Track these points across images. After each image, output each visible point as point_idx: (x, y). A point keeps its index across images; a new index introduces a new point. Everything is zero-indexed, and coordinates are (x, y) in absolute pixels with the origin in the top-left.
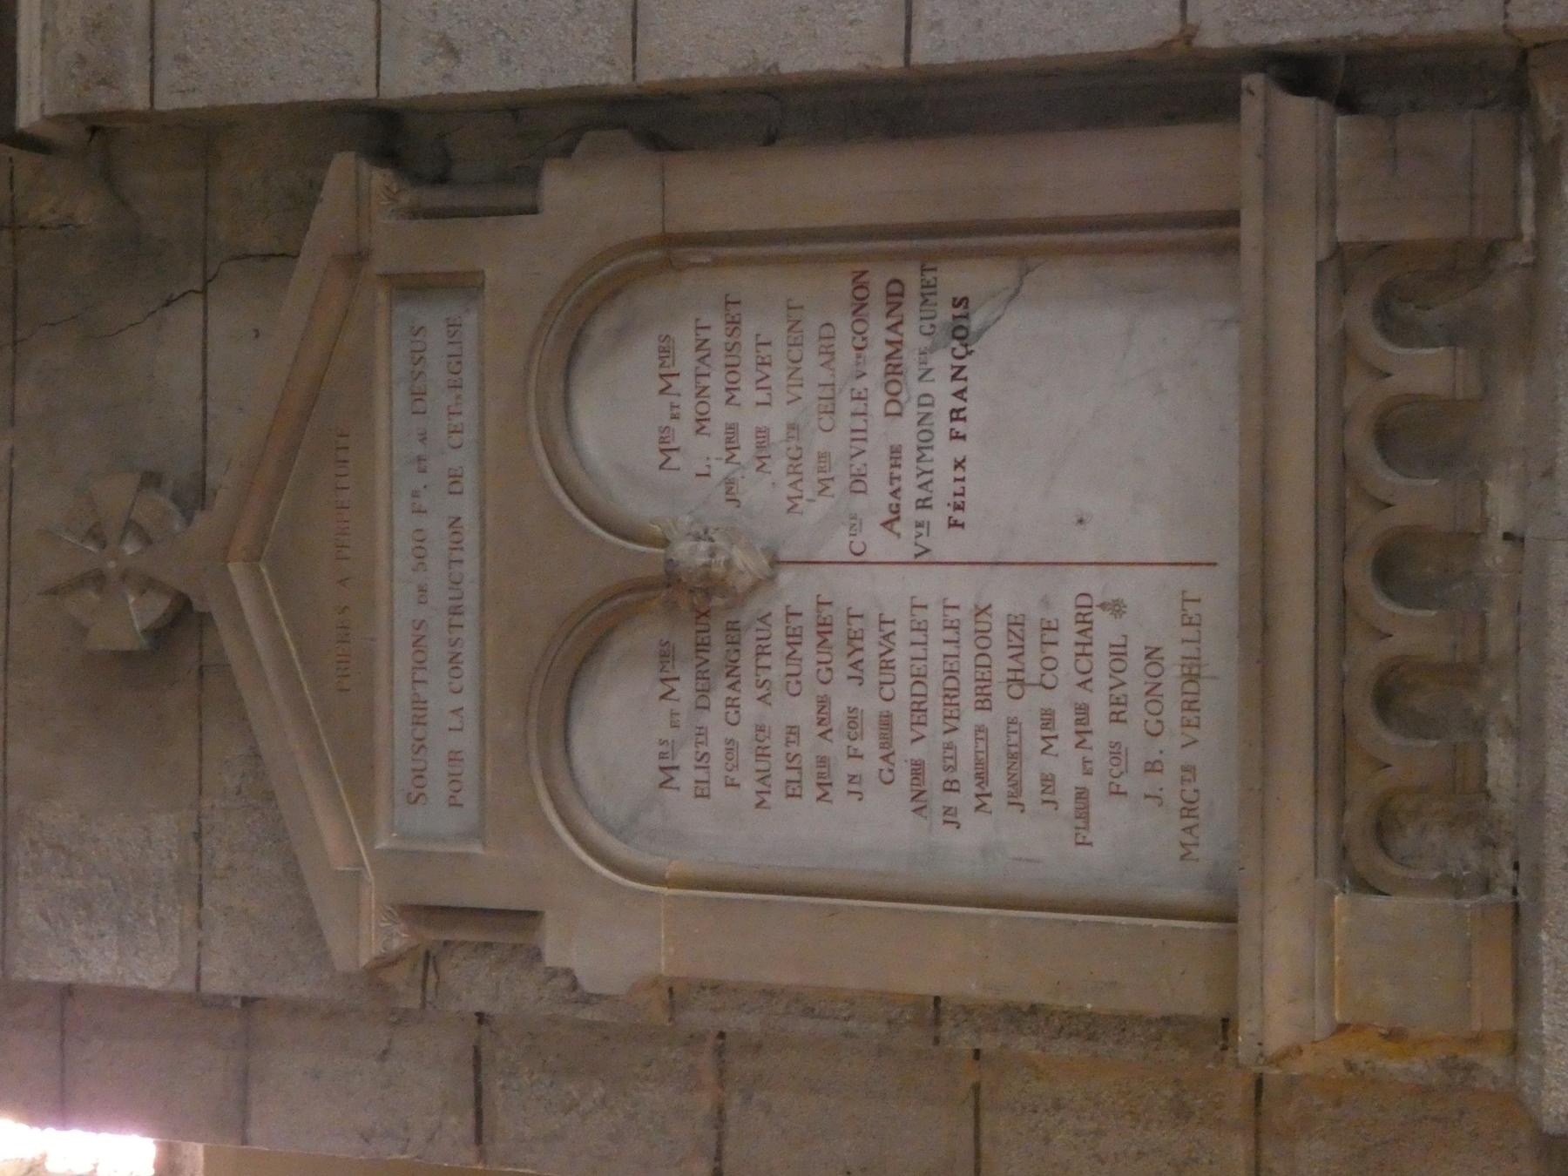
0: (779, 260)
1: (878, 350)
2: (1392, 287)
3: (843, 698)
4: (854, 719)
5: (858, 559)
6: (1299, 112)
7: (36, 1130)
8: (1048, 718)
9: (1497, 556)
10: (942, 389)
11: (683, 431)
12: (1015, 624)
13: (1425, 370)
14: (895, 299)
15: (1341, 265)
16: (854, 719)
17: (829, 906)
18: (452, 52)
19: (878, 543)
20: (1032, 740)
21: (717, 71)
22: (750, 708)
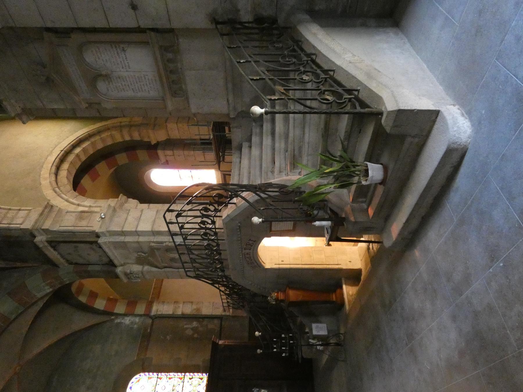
0: (111, 43)
1: (116, 52)
2: (164, 49)
3: (123, 83)
4: (125, 85)
5: (121, 71)
6: (152, 33)
7: (292, 238)
8: (143, 85)
9: (180, 70)
10: (124, 56)
11: (97, 60)
12: (138, 77)
13: (170, 56)
14: (116, 47)
15: (161, 47)
16: (125, 85)
17: (502, 191)
18: (54, 22)
19: (122, 70)
20: (143, 87)
21: (88, 27)
22: (114, 84)
